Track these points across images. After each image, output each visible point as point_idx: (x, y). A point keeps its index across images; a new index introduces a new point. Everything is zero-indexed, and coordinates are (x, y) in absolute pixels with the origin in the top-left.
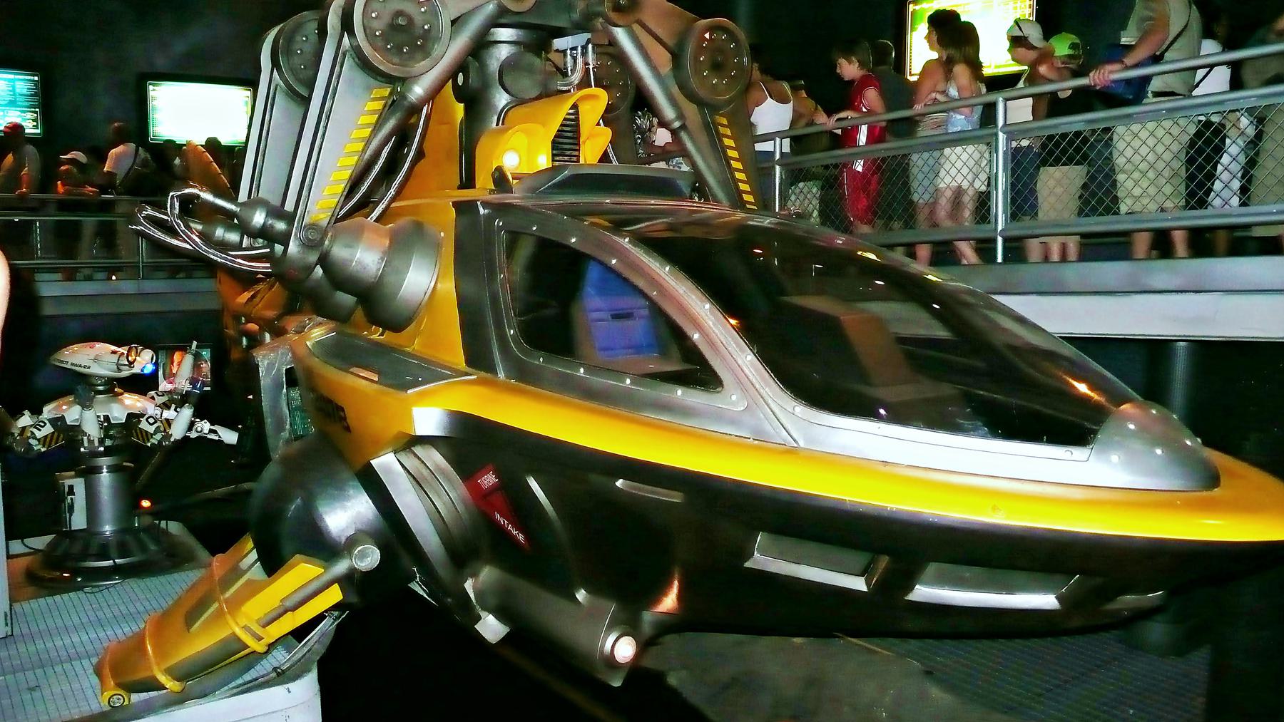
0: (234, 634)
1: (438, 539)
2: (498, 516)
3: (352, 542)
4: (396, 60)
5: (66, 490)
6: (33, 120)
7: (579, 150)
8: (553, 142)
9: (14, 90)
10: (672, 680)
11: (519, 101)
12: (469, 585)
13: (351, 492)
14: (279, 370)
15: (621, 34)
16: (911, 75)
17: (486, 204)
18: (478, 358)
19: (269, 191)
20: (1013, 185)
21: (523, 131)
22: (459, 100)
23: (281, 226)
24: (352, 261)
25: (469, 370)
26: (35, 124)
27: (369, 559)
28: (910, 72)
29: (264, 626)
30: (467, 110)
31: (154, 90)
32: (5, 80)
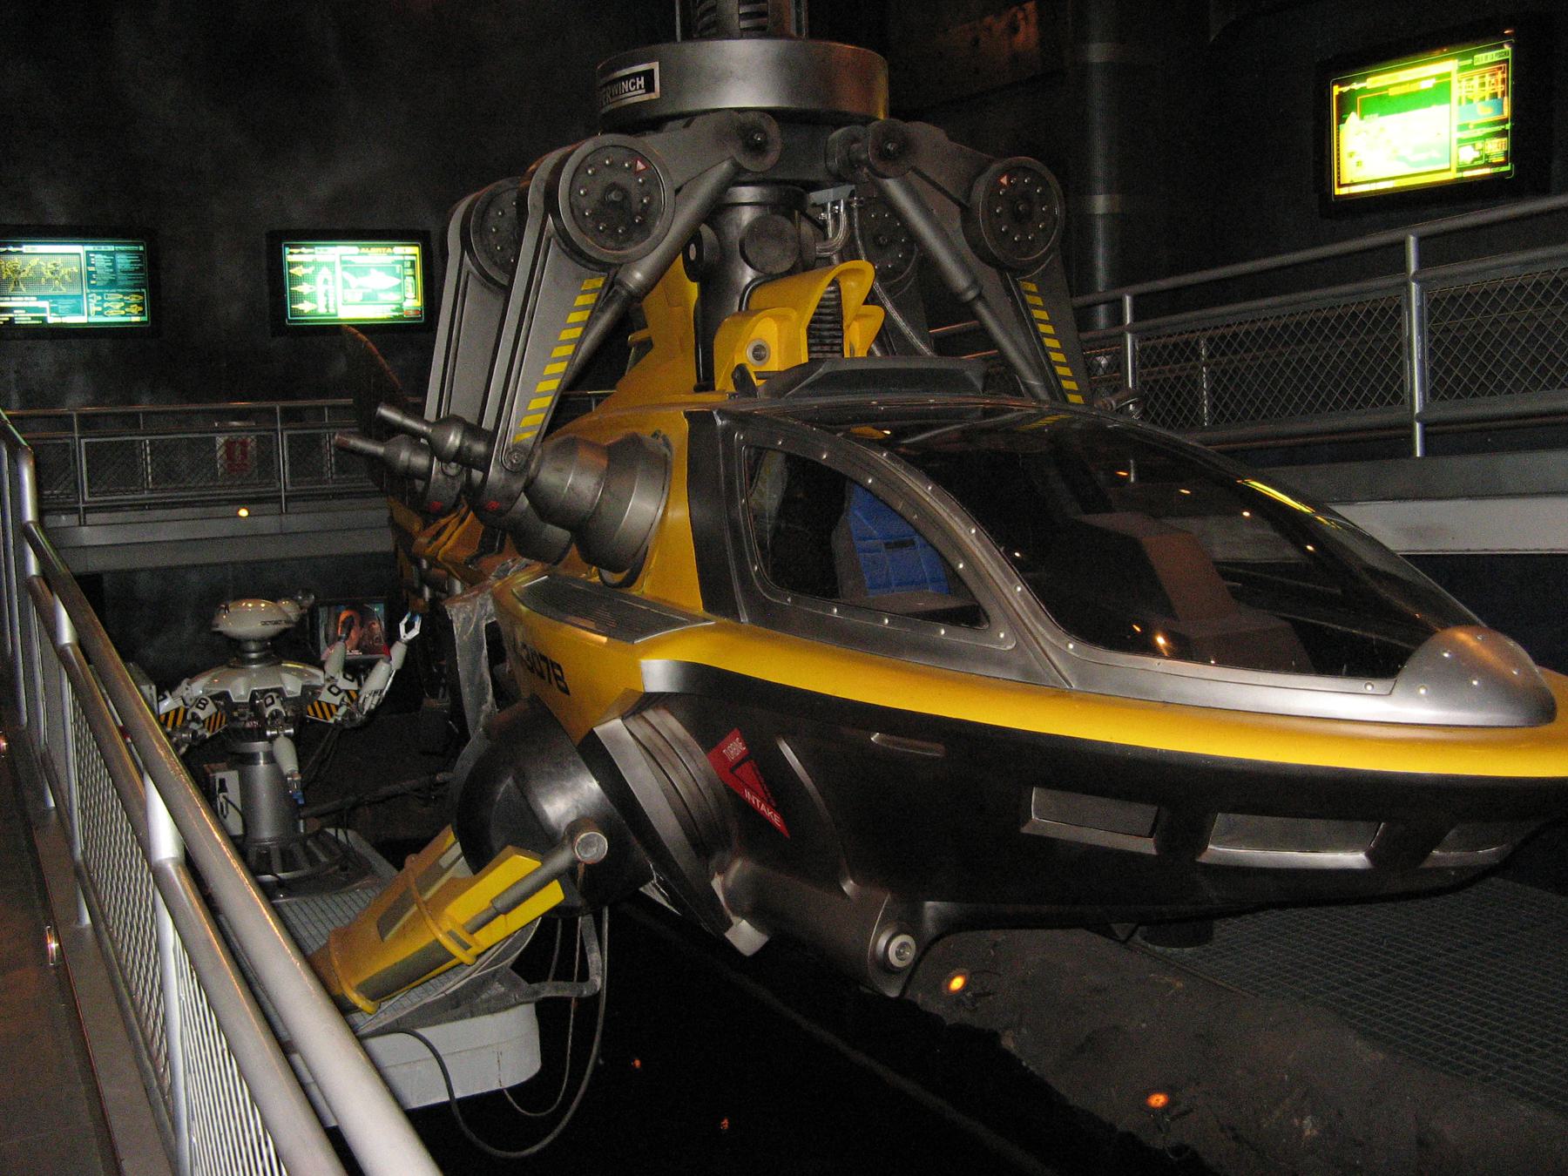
0: (437, 941)
1: (676, 822)
2: (748, 795)
3: (574, 828)
4: (610, 243)
5: (218, 786)
6: (139, 305)
7: (842, 337)
8: (809, 329)
9: (114, 266)
10: (1008, 1043)
11: (767, 278)
12: (717, 883)
13: (572, 769)
14: (477, 626)
15: (893, 187)
16: (1340, 186)
17: (724, 413)
18: (717, 597)
19: (462, 406)
20: (1432, 353)
21: (775, 317)
22: (693, 280)
23: (480, 448)
24: (563, 489)
25: (708, 615)
26: (141, 309)
27: (595, 848)
28: (1339, 182)
29: (472, 933)
30: (702, 292)
31: (291, 253)
32: (103, 253)
